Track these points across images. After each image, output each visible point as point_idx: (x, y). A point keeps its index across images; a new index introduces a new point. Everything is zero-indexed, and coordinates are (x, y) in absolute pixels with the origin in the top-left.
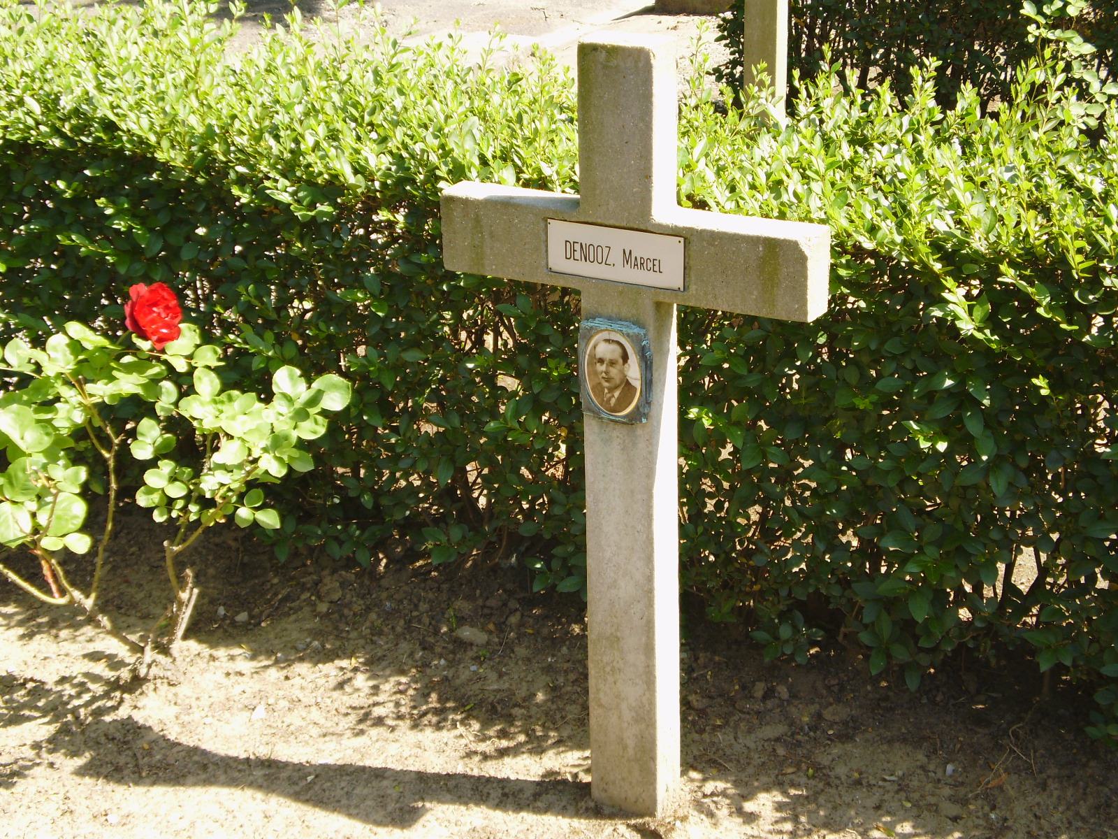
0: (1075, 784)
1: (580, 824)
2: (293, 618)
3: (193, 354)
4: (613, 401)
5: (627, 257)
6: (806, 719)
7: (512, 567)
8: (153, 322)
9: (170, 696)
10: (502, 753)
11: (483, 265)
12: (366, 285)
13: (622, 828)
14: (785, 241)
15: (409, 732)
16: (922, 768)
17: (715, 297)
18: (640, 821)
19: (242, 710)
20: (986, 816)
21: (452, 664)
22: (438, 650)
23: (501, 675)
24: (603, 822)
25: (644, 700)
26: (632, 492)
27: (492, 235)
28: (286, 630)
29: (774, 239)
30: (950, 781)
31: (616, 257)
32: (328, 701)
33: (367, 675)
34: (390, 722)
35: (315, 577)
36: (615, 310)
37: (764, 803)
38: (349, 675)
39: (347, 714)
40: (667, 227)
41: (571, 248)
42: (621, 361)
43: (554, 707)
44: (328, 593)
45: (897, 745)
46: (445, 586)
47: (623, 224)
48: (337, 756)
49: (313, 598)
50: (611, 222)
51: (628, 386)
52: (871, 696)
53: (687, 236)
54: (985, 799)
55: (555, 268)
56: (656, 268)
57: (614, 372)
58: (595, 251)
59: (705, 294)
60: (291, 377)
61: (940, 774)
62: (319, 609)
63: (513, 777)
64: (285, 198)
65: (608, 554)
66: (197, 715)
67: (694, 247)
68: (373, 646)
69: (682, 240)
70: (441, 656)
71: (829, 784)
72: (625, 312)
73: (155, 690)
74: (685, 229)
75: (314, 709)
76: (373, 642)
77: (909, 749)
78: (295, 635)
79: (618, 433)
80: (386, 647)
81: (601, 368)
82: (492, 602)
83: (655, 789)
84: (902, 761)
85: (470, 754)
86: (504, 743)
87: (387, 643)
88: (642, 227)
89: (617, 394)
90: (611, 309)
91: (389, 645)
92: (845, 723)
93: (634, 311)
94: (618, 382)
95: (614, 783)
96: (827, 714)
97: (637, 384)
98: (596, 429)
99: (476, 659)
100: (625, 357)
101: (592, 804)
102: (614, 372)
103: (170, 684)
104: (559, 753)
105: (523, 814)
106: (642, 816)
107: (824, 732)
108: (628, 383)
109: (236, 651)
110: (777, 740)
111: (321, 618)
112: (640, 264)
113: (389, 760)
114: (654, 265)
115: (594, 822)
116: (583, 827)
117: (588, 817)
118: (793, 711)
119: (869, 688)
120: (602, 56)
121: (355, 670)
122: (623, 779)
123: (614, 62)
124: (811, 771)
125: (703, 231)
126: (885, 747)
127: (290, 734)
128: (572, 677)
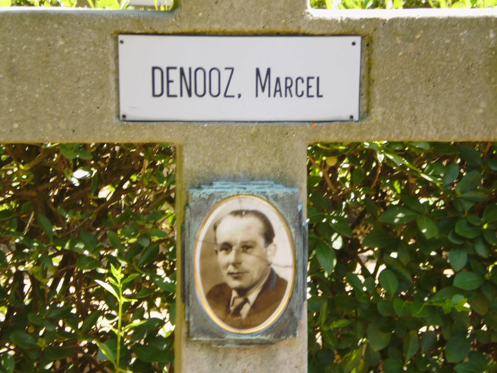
17: (415, 121)
36: (244, 165)
42: (261, 241)
47: (259, 27)
55: (132, 114)
56: (313, 91)
58: (207, 77)
59: (399, 118)
69: (358, 40)
88: (292, 28)
89: (252, 297)
93: (276, 163)
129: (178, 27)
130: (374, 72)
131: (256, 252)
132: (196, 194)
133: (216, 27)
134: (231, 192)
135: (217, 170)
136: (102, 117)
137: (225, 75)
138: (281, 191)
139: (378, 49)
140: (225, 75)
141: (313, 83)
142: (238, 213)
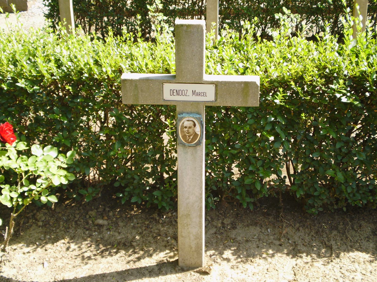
0: (307, 227)
1: (179, 275)
2: (31, 229)
3: (16, 146)
4: (190, 140)
5: (194, 93)
6: (220, 225)
7: (100, 197)
8: (8, 136)
9: (11, 266)
10: (139, 259)
11: (138, 101)
12: (55, 112)
13: (193, 273)
14: (251, 82)
15: (102, 259)
16: (261, 232)
17: (226, 102)
18: (198, 269)
19: (38, 265)
20: (289, 242)
21: (100, 233)
22: (93, 229)
23: (119, 233)
24: (186, 273)
25: (199, 232)
26: (195, 168)
27: (142, 91)
28: (31, 234)
29: (247, 82)
30: (271, 234)
31: (190, 93)
32: (66, 255)
33: (74, 244)
34: (93, 257)
35: (32, 214)
36: (190, 110)
37: (228, 254)
38: (68, 245)
39: (76, 258)
40: (209, 81)
41: (172, 92)
42: (193, 126)
43: (144, 239)
44: (40, 218)
45: (250, 227)
46: (81, 208)
47: (193, 82)
48: (85, 273)
49: (34, 221)
50: (188, 82)
51: (196, 135)
52: (234, 214)
53: (216, 84)
54: (284, 237)
55: (166, 99)
56: (205, 95)
57: (191, 130)
58: (182, 91)
59: (223, 101)
60: (37, 148)
61: (267, 233)
62: (39, 225)
63: (147, 266)
64: (23, 86)
65: (186, 189)
66: (24, 270)
67: (219, 87)
68: (68, 233)
69: (214, 85)
70: (95, 231)
71: (239, 243)
72: (193, 110)
73: (5, 264)
74: (215, 81)
75: (63, 258)
76: (68, 232)
77: (254, 227)
78: (36, 235)
79: (190, 150)
80: (73, 232)
81: (185, 130)
82: (100, 210)
83: (202, 259)
84: (255, 231)
85: (128, 262)
86: (137, 256)
87: (73, 231)
88: (200, 82)
89: (191, 137)
90: (188, 110)
91: (74, 231)
92: (232, 224)
93: (197, 110)
94: (192, 133)
95: (187, 260)
96: (225, 222)
97: (199, 133)
98: (182, 150)
99: (108, 229)
100: (195, 125)
101: (180, 268)
102: (191, 130)
103: (9, 262)
104: (157, 255)
105: (160, 277)
106: (198, 268)
107: (227, 228)
108: (196, 133)
109: (21, 245)
110: (216, 233)
111: (42, 227)
112: (199, 94)
113: (103, 270)
114: (204, 94)
115: (183, 273)
116: (181, 276)
117: (180, 272)
118: (214, 223)
119: (232, 211)
120: (185, 28)
121: (68, 243)
122: (191, 258)
123: (189, 30)
124: (232, 241)
125: (222, 82)
126: (247, 228)
127: (62, 269)
128: (144, 228)
129: (225, 37)
130: (218, 92)
131: (192, 129)
132: (179, 116)
133: (184, 82)
134: (186, 116)
135: (184, 111)
136: (160, 100)
137: (186, 91)
138: (198, 116)
139: (219, 87)
140: (186, 91)
141: (205, 93)
142: (188, 121)
